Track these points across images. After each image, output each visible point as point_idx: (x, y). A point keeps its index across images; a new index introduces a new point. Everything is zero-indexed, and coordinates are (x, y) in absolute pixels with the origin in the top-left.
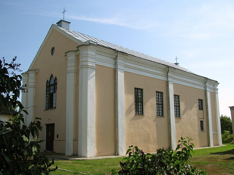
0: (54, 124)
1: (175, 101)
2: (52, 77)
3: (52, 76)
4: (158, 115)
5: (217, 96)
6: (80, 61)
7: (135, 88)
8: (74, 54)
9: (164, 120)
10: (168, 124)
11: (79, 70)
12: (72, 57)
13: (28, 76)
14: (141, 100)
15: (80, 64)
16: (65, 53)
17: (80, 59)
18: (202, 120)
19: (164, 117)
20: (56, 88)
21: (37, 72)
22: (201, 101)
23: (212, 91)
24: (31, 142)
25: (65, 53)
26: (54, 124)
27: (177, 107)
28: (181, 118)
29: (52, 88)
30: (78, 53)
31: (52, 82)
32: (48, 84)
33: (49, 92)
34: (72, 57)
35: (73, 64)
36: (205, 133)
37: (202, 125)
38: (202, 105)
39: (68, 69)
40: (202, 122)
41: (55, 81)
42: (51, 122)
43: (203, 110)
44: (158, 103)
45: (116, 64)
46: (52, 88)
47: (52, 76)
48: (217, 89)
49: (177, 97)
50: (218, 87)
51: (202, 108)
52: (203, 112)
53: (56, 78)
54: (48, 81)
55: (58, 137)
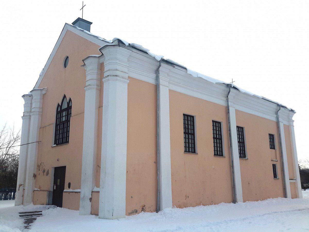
0: (65, 167)
1: (239, 134)
2: (65, 98)
3: (65, 97)
4: (216, 154)
5: (294, 150)
6: (105, 71)
7: (213, 121)
8: (96, 60)
9: (222, 162)
10: (231, 168)
11: (103, 85)
12: (91, 66)
13: (32, 99)
14: (192, 131)
15: (105, 74)
16: (83, 61)
17: (105, 68)
18: (274, 163)
19: (225, 157)
20: (71, 113)
21: (44, 92)
22: (271, 137)
23: (286, 123)
24: (35, 204)
25: (83, 61)
26: (65, 167)
27: (242, 143)
28: (248, 159)
29: (64, 114)
30: (101, 60)
31: (65, 106)
32: (59, 109)
33: (60, 120)
34: (91, 66)
35: (95, 76)
36: (279, 182)
37: (275, 169)
38: (273, 142)
39: (87, 84)
40: (274, 166)
41: (68, 104)
42: (61, 164)
43: (274, 149)
44: (215, 136)
45: (157, 78)
46: (64, 114)
47: (65, 97)
48: (293, 121)
49: (240, 130)
50: (294, 118)
51: (274, 145)
52: (276, 151)
53: (70, 100)
54: (59, 104)
55: (69, 187)
